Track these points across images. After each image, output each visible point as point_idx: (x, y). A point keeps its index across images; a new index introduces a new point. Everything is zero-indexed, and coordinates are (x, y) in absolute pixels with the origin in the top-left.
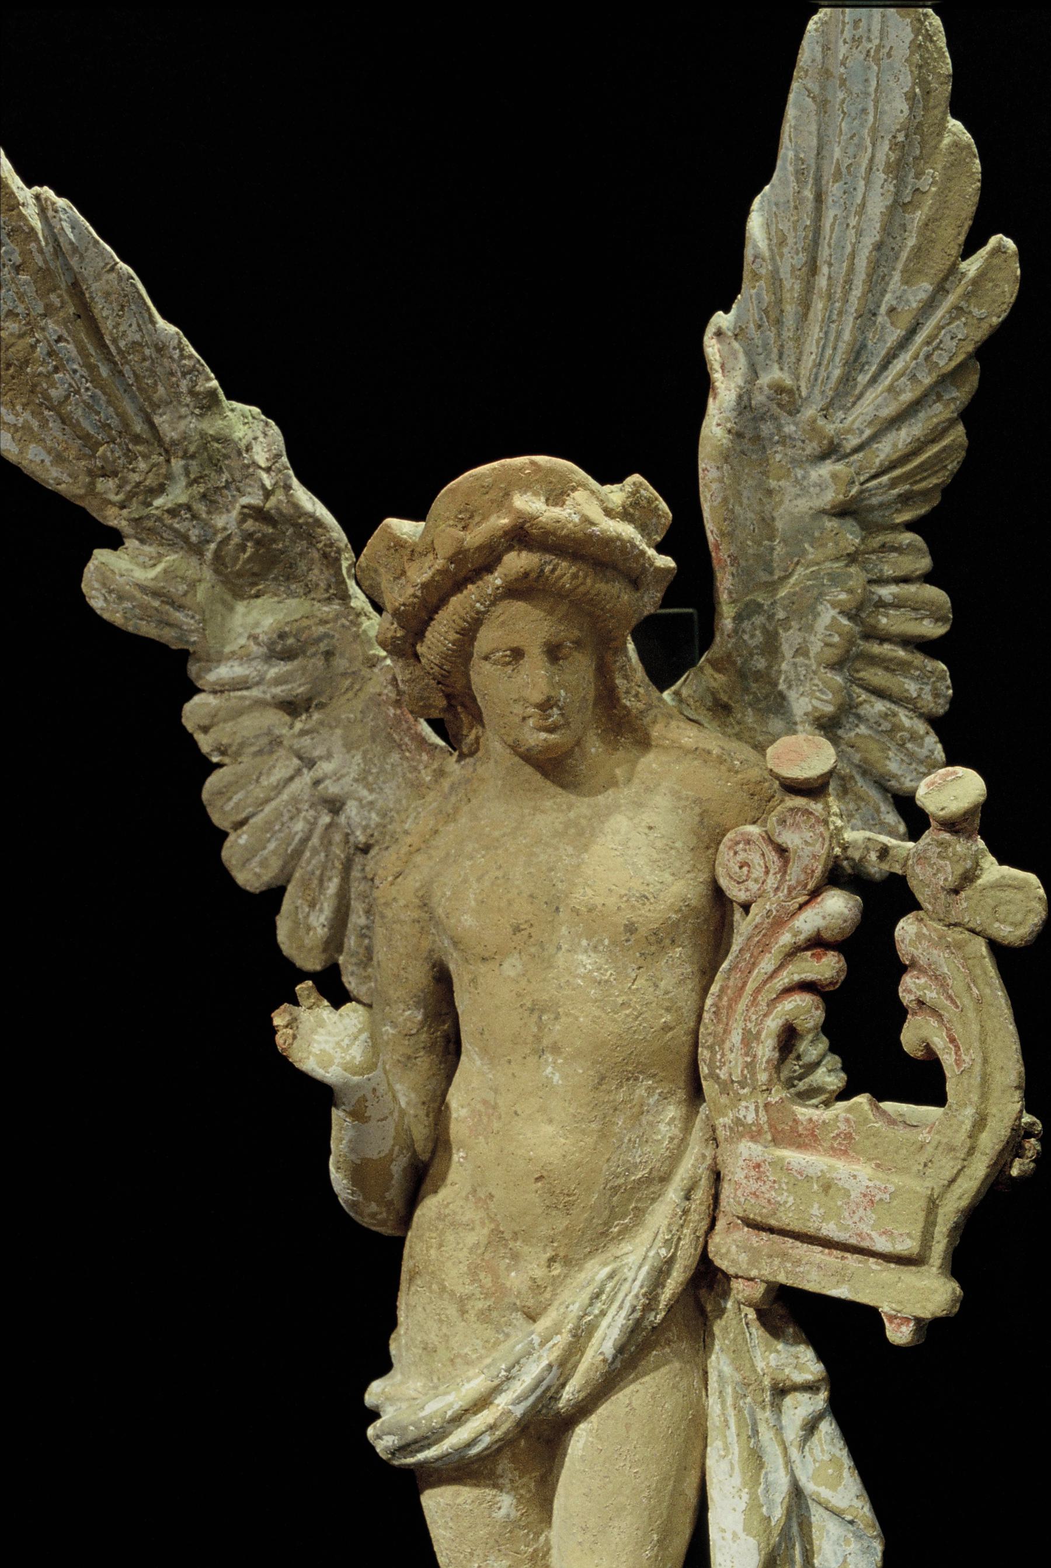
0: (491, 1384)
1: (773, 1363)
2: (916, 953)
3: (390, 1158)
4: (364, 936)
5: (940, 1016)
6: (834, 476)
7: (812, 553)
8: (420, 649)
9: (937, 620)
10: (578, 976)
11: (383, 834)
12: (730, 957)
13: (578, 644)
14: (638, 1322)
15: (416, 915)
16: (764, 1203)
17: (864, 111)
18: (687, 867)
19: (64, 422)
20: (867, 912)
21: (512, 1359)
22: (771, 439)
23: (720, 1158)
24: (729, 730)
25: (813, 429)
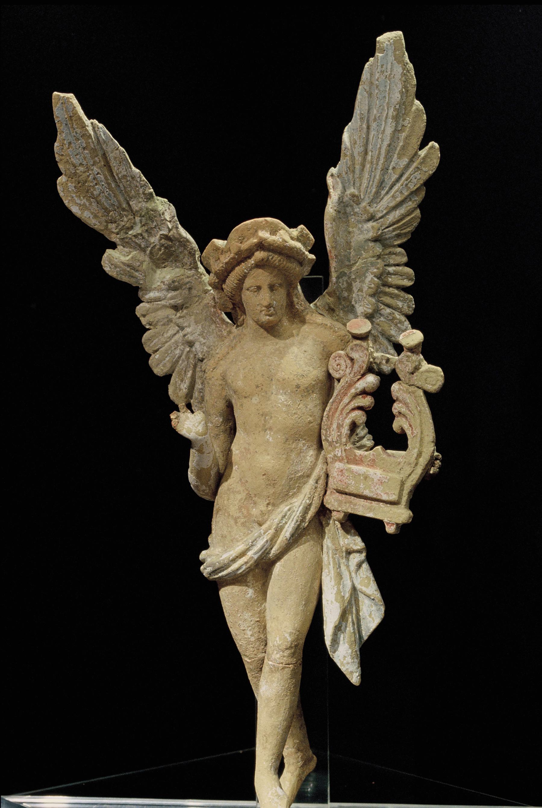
0: (245, 547)
1: (346, 543)
2: (398, 395)
3: (210, 468)
4: (201, 392)
5: (406, 417)
6: (373, 227)
7: (364, 255)
8: (224, 286)
9: (409, 280)
10: (279, 403)
11: (208, 354)
12: (333, 398)
13: (281, 285)
14: (299, 526)
15: (220, 383)
16: (344, 483)
17: (385, 97)
18: (318, 366)
19: (98, 203)
20: (381, 382)
21: (253, 539)
22: (350, 213)
23: (328, 470)
24: (334, 318)
25: (365, 210)
